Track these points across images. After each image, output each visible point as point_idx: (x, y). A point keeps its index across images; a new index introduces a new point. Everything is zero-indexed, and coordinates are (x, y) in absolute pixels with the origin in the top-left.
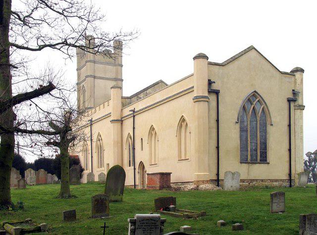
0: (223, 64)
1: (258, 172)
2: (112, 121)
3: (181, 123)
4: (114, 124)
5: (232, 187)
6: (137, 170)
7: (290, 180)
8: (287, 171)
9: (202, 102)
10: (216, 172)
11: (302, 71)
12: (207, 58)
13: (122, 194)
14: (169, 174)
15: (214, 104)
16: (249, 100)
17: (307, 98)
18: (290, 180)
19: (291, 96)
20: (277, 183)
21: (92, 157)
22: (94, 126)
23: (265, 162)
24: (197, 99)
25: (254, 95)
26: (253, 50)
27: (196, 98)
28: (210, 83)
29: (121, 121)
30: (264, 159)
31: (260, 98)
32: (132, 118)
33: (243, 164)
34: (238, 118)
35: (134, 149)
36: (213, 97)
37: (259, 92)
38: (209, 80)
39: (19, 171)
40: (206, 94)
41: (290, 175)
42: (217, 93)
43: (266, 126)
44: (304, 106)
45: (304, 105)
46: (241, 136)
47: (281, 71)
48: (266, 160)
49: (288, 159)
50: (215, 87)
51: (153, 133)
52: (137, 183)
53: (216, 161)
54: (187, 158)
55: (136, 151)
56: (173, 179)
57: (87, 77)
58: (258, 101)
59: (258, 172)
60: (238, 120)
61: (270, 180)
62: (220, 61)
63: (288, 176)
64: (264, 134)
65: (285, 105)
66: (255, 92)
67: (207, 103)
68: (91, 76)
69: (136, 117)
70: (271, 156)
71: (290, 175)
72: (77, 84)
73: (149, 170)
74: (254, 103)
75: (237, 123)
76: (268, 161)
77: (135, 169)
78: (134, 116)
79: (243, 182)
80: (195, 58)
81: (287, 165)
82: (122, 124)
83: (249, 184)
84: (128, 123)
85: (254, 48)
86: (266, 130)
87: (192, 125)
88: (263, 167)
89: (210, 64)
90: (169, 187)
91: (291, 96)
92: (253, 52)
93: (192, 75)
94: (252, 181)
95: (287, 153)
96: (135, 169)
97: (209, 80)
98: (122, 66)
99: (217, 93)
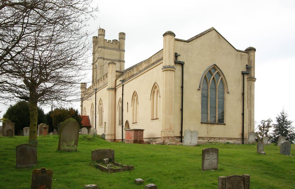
0: (188, 41)
1: (216, 131)
2: (109, 89)
3: (154, 89)
4: (110, 91)
5: (190, 143)
6: (124, 127)
7: (243, 138)
8: (240, 131)
9: (169, 72)
10: (180, 130)
11: (254, 50)
12: (174, 35)
13: (77, 145)
14: (142, 130)
15: (180, 73)
16: (210, 71)
17: (258, 72)
18: (243, 138)
19: (245, 70)
20: (223, 141)
21: (96, 117)
22: (98, 94)
23: (223, 123)
24: (166, 69)
25: (214, 68)
26: (214, 31)
27: (164, 67)
28: (176, 56)
29: (115, 89)
30: (221, 121)
31: (218, 70)
32: (122, 86)
33: (204, 125)
34: (200, 86)
35: (122, 111)
36: (178, 68)
37: (217, 65)
38: (175, 53)
39: (14, 123)
40: (172, 64)
41: (243, 134)
42: (182, 64)
43: (224, 94)
44: (256, 79)
45: (255, 78)
46: (202, 101)
47: (237, 49)
48: (223, 122)
49: (241, 121)
50: (180, 59)
51: (135, 98)
52: (124, 138)
53: (180, 121)
54: (158, 118)
55: (95, 103)
56: (145, 135)
57: (99, 58)
58: (218, 73)
59: (216, 131)
60: (200, 88)
61: (226, 138)
62: (186, 39)
63: (241, 135)
64: (222, 100)
65: (241, 76)
66: (215, 65)
67: (173, 72)
68: (101, 58)
69: (124, 86)
70: (227, 119)
71: (243, 134)
72: (93, 64)
73: (132, 127)
74: (214, 74)
75: (198, 90)
76: (225, 123)
77: (122, 126)
78: (123, 85)
79: (203, 139)
80: (164, 35)
81: (241, 125)
82: (115, 91)
83: (208, 141)
84: (119, 90)
85: (215, 29)
86: (224, 96)
87: (162, 88)
88: (220, 127)
89: (178, 40)
90: (141, 142)
91: (245, 70)
92: (213, 33)
93: (163, 49)
94: (211, 138)
95: (241, 116)
96: (122, 126)
97: (176, 54)
98: (124, 51)
99: (182, 64)
